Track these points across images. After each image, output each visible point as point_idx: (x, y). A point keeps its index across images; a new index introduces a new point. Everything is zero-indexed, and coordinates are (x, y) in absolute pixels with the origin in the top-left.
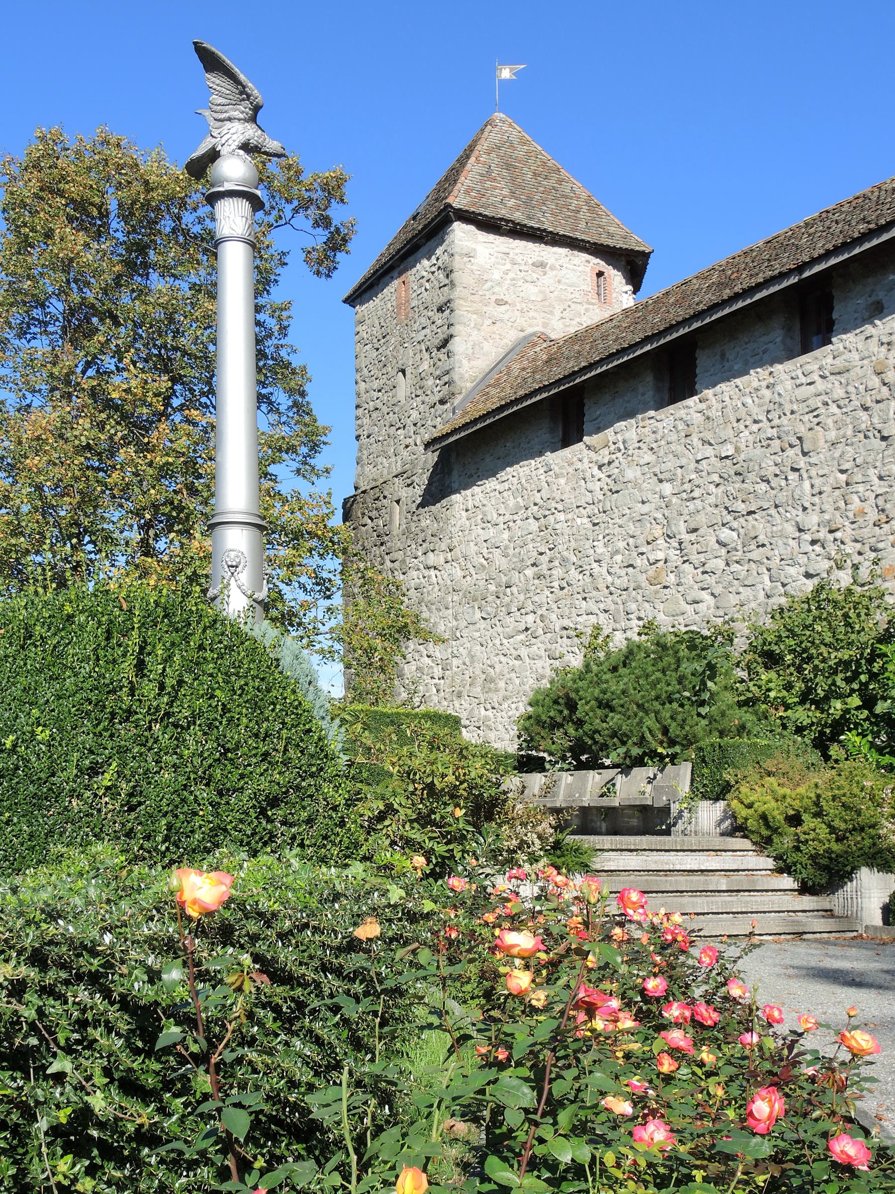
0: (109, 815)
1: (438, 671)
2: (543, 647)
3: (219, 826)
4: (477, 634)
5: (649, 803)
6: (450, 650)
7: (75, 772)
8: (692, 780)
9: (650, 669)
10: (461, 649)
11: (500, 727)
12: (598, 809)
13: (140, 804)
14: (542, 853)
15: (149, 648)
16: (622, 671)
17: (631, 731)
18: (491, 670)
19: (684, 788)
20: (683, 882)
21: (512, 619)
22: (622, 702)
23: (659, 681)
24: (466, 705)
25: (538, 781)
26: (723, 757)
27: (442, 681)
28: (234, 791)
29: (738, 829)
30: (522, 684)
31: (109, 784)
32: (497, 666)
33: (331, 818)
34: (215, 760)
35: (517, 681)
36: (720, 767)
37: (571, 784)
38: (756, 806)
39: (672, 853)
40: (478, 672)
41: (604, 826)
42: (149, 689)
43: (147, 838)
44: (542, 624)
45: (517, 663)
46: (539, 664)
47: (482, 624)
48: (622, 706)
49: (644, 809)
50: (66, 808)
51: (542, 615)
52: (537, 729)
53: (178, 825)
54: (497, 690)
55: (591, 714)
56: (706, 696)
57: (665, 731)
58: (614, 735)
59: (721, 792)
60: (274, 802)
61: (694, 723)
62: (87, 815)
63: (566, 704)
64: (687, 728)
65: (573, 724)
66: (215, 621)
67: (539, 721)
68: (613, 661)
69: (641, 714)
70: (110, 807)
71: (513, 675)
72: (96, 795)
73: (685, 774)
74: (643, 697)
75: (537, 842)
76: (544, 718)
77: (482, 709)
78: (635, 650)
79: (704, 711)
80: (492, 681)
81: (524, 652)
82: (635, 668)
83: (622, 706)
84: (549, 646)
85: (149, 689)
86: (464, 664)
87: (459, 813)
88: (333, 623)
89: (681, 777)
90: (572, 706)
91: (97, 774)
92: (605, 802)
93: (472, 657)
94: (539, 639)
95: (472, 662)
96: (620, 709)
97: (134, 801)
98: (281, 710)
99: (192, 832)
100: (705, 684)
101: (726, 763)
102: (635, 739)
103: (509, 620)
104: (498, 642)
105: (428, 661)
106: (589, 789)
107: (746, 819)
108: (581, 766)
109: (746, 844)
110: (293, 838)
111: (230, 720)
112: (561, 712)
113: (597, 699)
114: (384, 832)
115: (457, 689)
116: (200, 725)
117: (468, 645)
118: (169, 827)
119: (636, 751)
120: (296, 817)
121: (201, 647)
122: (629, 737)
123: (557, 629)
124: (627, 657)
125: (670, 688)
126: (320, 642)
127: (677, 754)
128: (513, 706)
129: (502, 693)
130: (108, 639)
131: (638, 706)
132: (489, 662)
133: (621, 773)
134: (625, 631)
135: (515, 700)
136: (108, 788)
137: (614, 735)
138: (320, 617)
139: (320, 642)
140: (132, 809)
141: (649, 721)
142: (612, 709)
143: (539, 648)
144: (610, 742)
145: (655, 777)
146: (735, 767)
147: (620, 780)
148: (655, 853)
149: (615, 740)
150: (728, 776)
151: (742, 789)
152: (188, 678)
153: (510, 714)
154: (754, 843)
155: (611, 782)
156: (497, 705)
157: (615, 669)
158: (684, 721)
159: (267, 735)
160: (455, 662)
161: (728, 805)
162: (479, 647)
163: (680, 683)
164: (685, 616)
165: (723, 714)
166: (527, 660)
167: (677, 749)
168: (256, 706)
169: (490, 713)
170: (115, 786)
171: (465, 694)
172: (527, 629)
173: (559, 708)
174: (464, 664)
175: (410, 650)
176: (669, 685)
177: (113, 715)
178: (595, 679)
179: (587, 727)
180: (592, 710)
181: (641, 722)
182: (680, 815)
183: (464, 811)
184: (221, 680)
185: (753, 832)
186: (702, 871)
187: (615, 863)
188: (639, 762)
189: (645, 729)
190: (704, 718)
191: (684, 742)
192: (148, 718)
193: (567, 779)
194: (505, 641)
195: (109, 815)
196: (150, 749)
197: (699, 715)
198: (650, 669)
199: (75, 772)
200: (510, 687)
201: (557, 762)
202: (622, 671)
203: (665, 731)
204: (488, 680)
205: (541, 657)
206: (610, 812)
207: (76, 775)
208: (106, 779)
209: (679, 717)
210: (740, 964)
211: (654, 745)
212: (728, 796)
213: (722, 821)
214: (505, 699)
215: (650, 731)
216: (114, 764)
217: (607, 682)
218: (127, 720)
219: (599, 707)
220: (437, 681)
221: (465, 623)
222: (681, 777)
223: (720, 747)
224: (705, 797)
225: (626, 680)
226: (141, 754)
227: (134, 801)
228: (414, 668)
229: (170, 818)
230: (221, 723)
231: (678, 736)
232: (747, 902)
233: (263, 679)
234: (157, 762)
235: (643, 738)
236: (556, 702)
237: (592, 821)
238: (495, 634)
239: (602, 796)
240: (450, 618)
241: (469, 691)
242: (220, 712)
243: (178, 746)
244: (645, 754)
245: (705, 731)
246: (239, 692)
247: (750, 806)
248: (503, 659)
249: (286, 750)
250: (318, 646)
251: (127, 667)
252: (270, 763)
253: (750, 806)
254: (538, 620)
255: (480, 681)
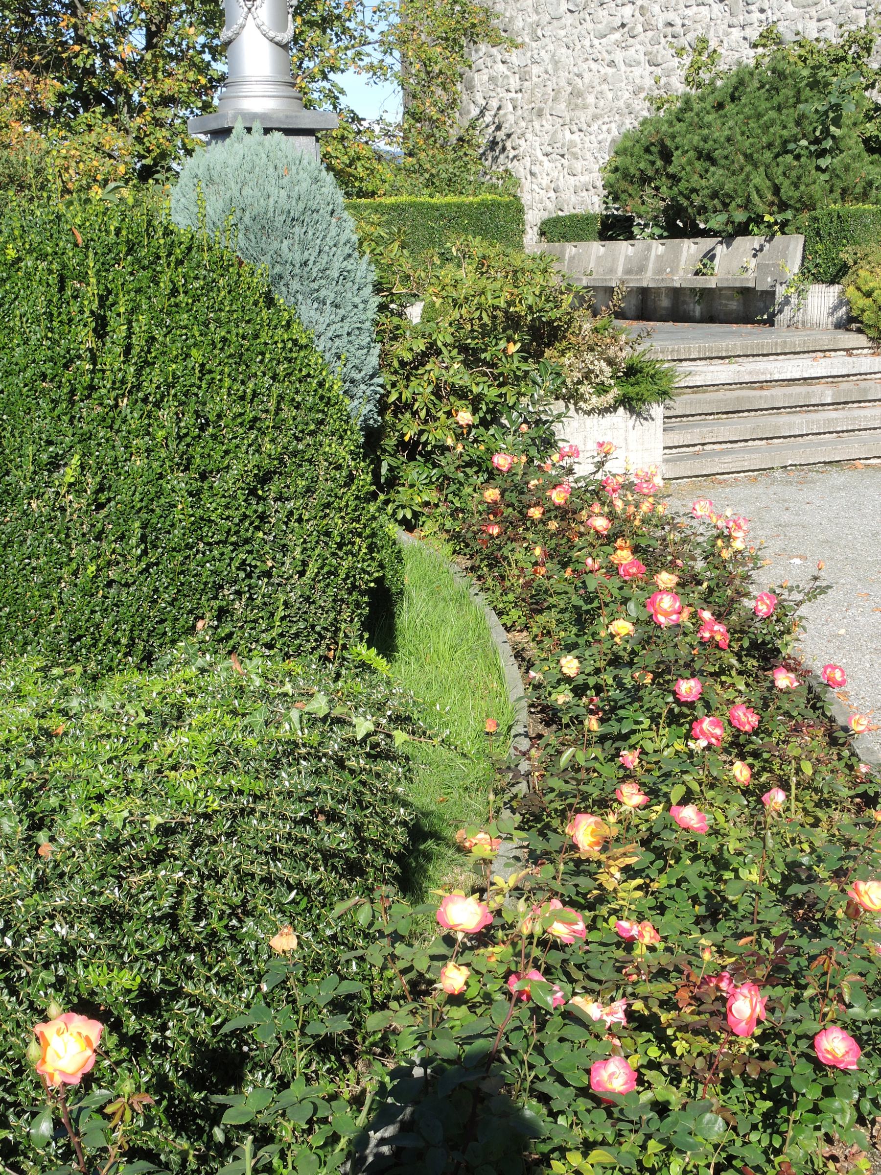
0: (75, 517)
1: (514, 82)
2: (642, 49)
3: (202, 518)
4: (562, 33)
5: (751, 285)
6: (529, 54)
7: (32, 468)
8: (804, 258)
9: (763, 105)
10: (543, 53)
11: (588, 155)
12: (693, 290)
13: (109, 500)
14: (612, 382)
15: (111, 299)
16: (730, 108)
17: (735, 191)
18: (578, 80)
19: (793, 267)
20: (778, 396)
21: (605, 12)
22: (726, 152)
23: (773, 123)
24: (548, 127)
25: (623, 251)
26: (842, 230)
27: (519, 95)
28: (218, 472)
29: (850, 322)
30: (616, 98)
31: (72, 480)
32: (587, 76)
33: (334, 480)
34: (193, 438)
35: (610, 95)
36: (837, 242)
37: (661, 256)
38: (875, 294)
39: (772, 358)
40: (563, 83)
41: (698, 309)
42: (112, 358)
43: (122, 538)
44: (642, 19)
45: (610, 71)
46: (637, 71)
47: (569, 19)
48: (726, 158)
49: (745, 292)
50: (24, 512)
51: (642, 7)
52: (624, 185)
53: (154, 521)
54: (585, 107)
55: (688, 168)
56: (828, 144)
57: (776, 190)
58: (714, 195)
59: (837, 274)
60: (265, 478)
61: (811, 180)
62: (49, 520)
63: (660, 152)
64: (802, 188)
65: (665, 181)
66: (190, 249)
67: (627, 176)
68: (718, 96)
69: (748, 168)
70: (75, 506)
71: (605, 87)
72: (58, 493)
73: (795, 249)
74: (752, 145)
75: (608, 370)
76: (632, 171)
77: (567, 132)
78: (747, 79)
79: (824, 163)
80: (580, 94)
81: (619, 56)
82: (745, 105)
83: (726, 158)
84: (650, 48)
85: (112, 358)
86: (546, 72)
87: (513, 348)
88: (383, 26)
89: (791, 250)
90: (666, 156)
91: (58, 466)
92: (701, 282)
93: (556, 63)
94: (638, 39)
95: (556, 70)
96: (723, 162)
97: (103, 498)
98: (271, 360)
99: (173, 525)
100: (828, 129)
101: (845, 237)
102: (739, 201)
103: (602, 13)
104: (587, 43)
105: (501, 68)
106: (682, 263)
107: (863, 311)
108: (674, 232)
109: (861, 340)
110: (291, 513)
111: (211, 383)
112: (653, 163)
113: (696, 149)
114: (426, 377)
115: (538, 105)
116: (175, 395)
117: (551, 47)
118: (144, 526)
119: (740, 216)
120: (292, 489)
121: (174, 292)
122: (732, 198)
123: (660, 26)
124: (736, 88)
125: (785, 133)
126: (369, 55)
127: (788, 221)
128: (605, 128)
129: (591, 110)
130: (62, 289)
131: (745, 156)
132: (576, 70)
133: (721, 243)
134: (743, 27)
135: (606, 120)
136: (71, 485)
137: (714, 195)
138: (367, 21)
139: (369, 55)
140: (100, 506)
141: (758, 179)
142: (714, 162)
143: (637, 51)
144: (710, 205)
145: (761, 250)
146: (856, 243)
147: (721, 250)
148: (751, 359)
149: (716, 201)
150: (846, 255)
151: (862, 273)
152: (158, 333)
153: (600, 138)
154: (872, 339)
155: (710, 256)
156: (584, 127)
157: (720, 106)
158: (799, 178)
159: (255, 394)
160: (535, 70)
161: (843, 292)
162: (564, 50)
163: (798, 123)
164: (819, 7)
165: (847, 168)
166: (623, 68)
167: (789, 214)
168: (240, 358)
169: (576, 137)
170: (78, 482)
171: (547, 111)
172: (623, 25)
173: (651, 158)
174: (546, 72)
175: (481, 54)
176: (785, 127)
177: (72, 392)
178: (696, 119)
179: (683, 185)
180: (690, 163)
181: (748, 178)
182: (787, 301)
183: (519, 345)
184: (197, 334)
185: (870, 326)
186: (805, 379)
187: (702, 377)
188: (743, 230)
189: (752, 189)
190: (824, 171)
191: (798, 205)
192: (113, 394)
193: (658, 248)
194: (596, 42)
195: (75, 517)
196: (118, 431)
197: (818, 168)
198: (763, 105)
199: (32, 468)
200: (602, 103)
201: (646, 225)
202: (730, 108)
203: (776, 190)
204: (576, 94)
205: (639, 63)
206: (705, 294)
207: (35, 472)
208: (69, 474)
209: (794, 174)
210: (803, 610)
211: (761, 208)
212: (844, 280)
213: (835, 309)
214: (595, 118)
215: (758, 191)
216: (77, 457)
217: (709, 126)
218: (89, 397)
219: (699, 159)
220: (513, 95)
221: (547, 18)
222: (791, 250)
223: (839, 217)
224: (817, 279)
225: (731, 123)
226: (107, 440)
227: (103, 498)
228: (486, 78)
229: (144, 515)
230: (199, 387)
231: (791, 198)
232: (855, 418)
233: (248, 322)
234: (126, 447)
235: (748, 199)
236: (647, 150)
237: (684, 302)
238: (584, 33)
239: (697, 273)
240: (530, 10)
241: (552, 108)
242: (198, 374)
243: (149, 425)
244: (750, 220)
245: (823, 189)
246: (219, 346)
247: (868, 294)
248: (594, 66)
249: (278, 410)
250: (367, 60)
251: (85, 337)
252: (259, 429)
253: (868, 294)
254: (637, 14)
255: (565, 95)
